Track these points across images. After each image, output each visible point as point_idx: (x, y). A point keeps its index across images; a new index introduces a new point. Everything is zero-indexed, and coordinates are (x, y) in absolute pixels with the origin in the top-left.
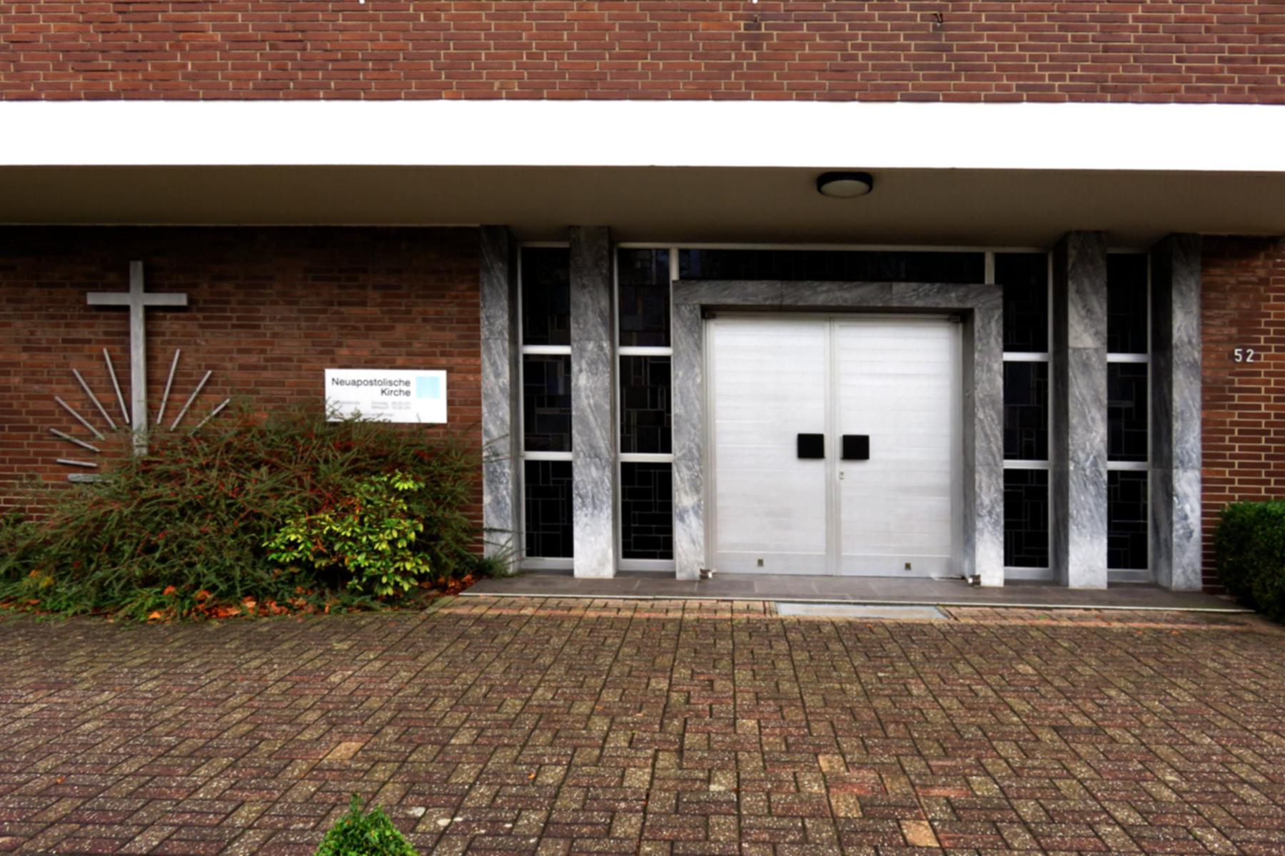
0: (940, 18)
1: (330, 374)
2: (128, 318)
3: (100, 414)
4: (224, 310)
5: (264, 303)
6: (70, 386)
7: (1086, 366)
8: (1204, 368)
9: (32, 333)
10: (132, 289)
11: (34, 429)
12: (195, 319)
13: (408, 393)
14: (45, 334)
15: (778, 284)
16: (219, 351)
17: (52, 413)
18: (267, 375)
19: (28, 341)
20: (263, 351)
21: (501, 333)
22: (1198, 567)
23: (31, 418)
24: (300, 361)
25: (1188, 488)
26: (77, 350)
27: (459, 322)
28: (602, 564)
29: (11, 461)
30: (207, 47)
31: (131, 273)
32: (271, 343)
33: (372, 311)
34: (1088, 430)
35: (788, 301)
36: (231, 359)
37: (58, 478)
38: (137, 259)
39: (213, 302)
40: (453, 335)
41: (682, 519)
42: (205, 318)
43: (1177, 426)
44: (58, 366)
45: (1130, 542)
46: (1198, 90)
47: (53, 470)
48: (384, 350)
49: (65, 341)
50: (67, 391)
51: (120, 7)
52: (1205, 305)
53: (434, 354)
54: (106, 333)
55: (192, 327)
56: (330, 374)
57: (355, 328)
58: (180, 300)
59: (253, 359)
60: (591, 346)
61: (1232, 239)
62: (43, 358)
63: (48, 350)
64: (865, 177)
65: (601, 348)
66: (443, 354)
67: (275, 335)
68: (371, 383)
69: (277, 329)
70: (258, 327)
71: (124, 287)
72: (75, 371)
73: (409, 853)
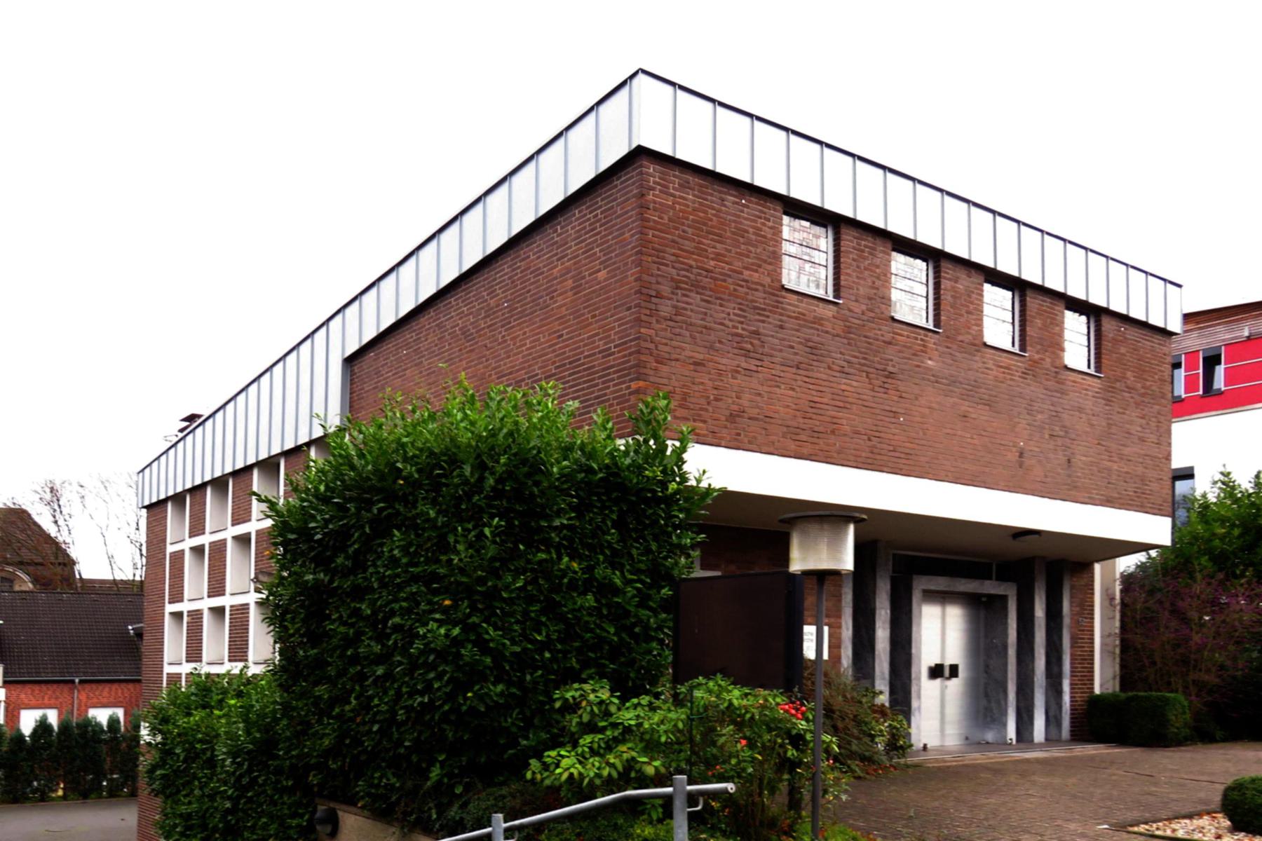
52: (1072, 597)
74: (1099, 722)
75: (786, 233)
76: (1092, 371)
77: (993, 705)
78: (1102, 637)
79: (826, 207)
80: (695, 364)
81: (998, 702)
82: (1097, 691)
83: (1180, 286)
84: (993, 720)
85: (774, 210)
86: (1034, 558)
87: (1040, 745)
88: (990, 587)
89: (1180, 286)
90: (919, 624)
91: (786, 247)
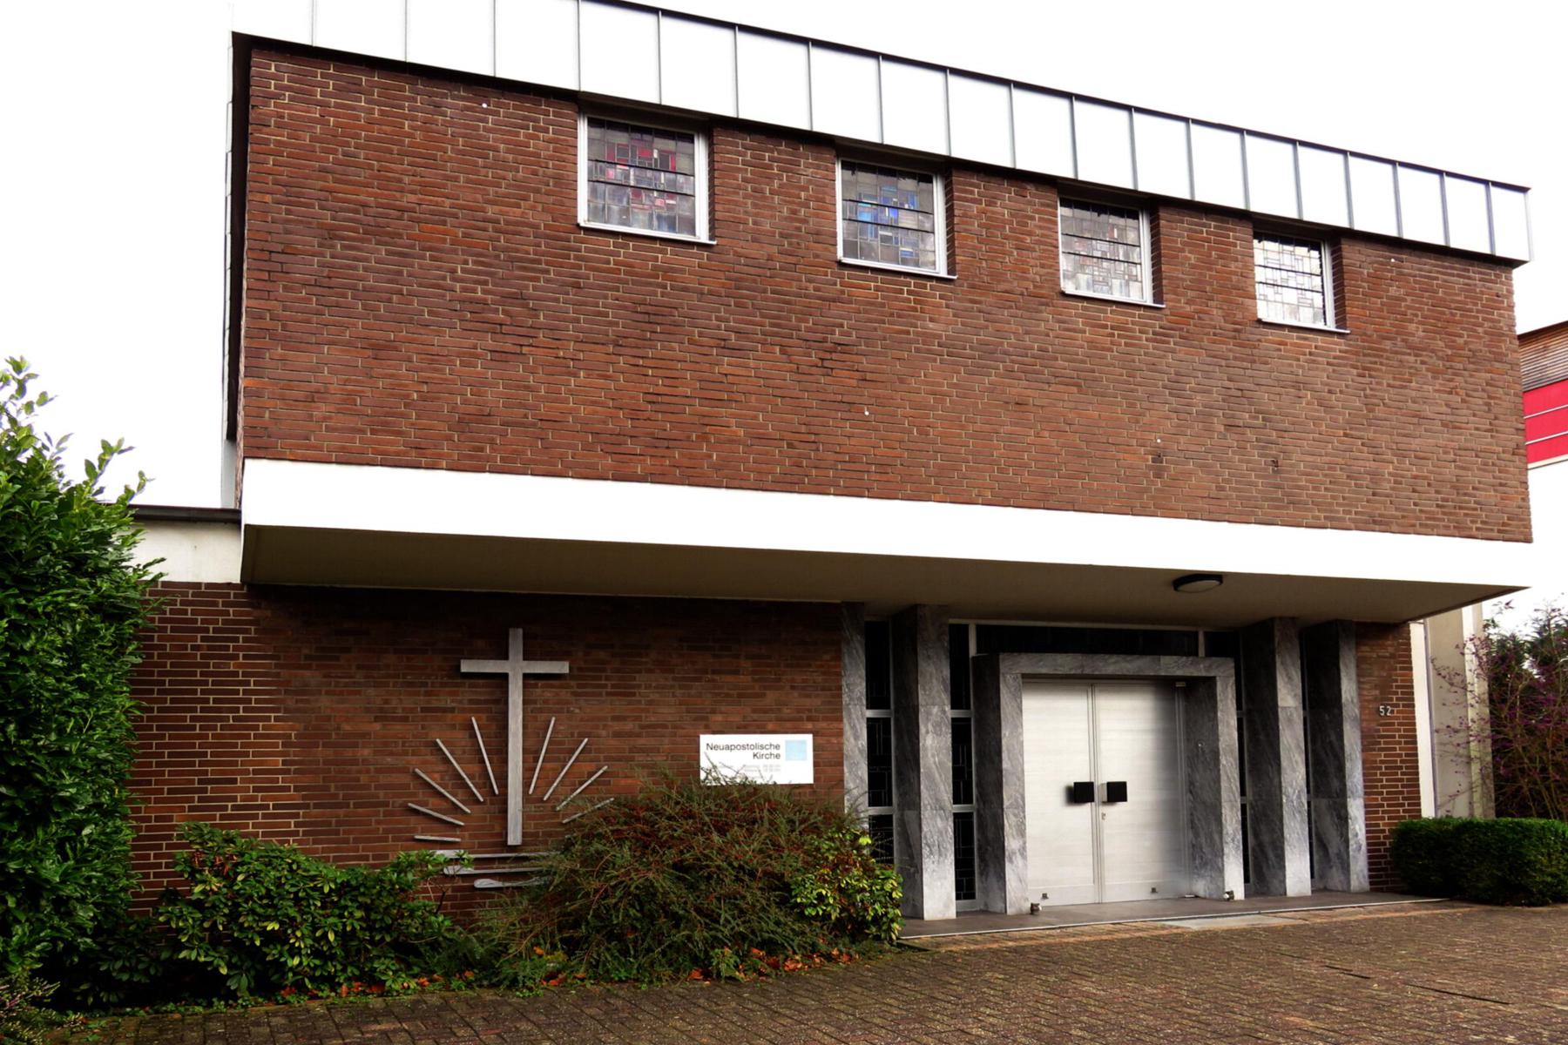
0: (1275, 463)
1: (705, 739)
5: (639, 672)
6: (429, 758)
7: (1290, 720)
8: (1362, 721)
9: (386, 702)
11: (386, 804)
12: (568, 687)
13: (778, 756)
15: (1079, 656)
18: (641, 741)
20: (638, 718)
21: (859, 699)
22: (1366, 872)
23: (381, 793)
24: (675, 727)
25: (1356, 809)
27: (823, 689)
28: (947, 906)
29: (356, 840)
30: (731, 441)
31: (511, 640)
33: (744, 679)
34: (1294, 770)
35: (1087, 671)
36: (605, 727)
40: (818, 702)
41: (1011, 861)
42: (579, 686)
43: (1348, 765)
44: (415, 736)
45: (1326, 854)
46: (1426, 526)
48: (755, 716)
50: (425, 762)
51: (650, 398)
52: (1360, 674)
53: (801, 719)
54: (471, 701)
55: (565, 694)
56: (705, 739)
57: (728, 695)
58: (562, 667)
59: (629, 726)
60: (935, 710)
61: (1374, 624)
62: (398, 727)
63: (405, 719)
64: (1218, 577)
65: (944, 712)
66: (809, 719)
67: (651, 703)
68: (744, 747)
69: (652, 697)
70: (634, 694)
71: (504, 655)
74: (1423, 863)
75: (1259, 258)
76: (1331, 326)
77: (1203, 840)
78: (1434, 731)
79: (1306, 218)
80: (374, 347)
81: (1210, 836)
82: (1428, 810)
83: (1523, 190)
84: (1204, 864)
85: (1238, 234)
86: (1272, 619)
87: (1300, 900)
88: (1198, 669)
89: (1523, 190)
90: (1018, 725)
91: (1260, 274)
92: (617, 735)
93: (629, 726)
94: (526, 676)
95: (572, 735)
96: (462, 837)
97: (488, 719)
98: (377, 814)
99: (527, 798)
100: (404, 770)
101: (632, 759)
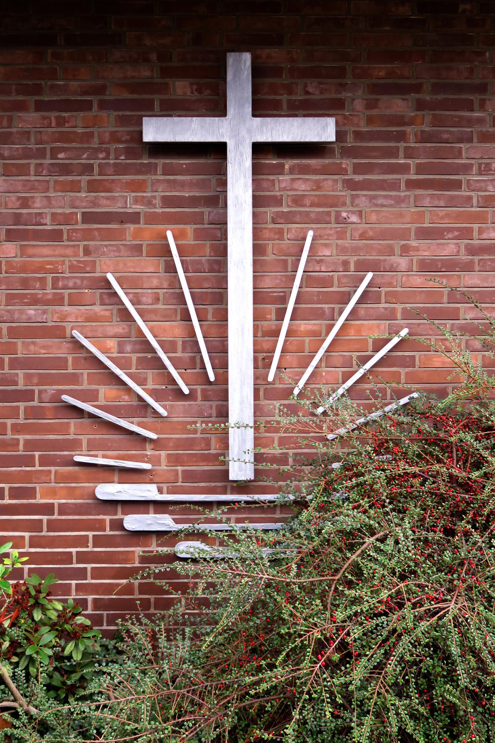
2: (221, 172)
3: (159, 364)
4: (393, 153)
6: (98, 309)
9: (25, 203)
10: (231, 110)
11: (27, 395)
14: (51, 203)
16: (383, 235)
17: (62, 363)
18: (471, 280)
19: (17, 219)
20: (466, 234)
26: (108, 236)
32: (480, 218)
36: (405, 250)
37: (71, 492)
38: (239, 48)
39: (373, 136)
42: (357, 169)
44: (73, 269)
47: (60, 478)
49: (88, 218)
54: (167, 201)
55: (332, 186)
58: (320, 130)
59: (448, 249)
62: (44, 252)
63: (56, 236)
70: (457, 185)
71: (218, 108)
72: (110, 277)
73: (290, 741)
92: (428, 267)
93: (448, 249)
94: (259, 149)
95: (346, 264)
96: (155, 461)
97: (198, 234)
98: (14, 414)
99: (262, 391)
100: (57, 332)
101: (454, 315)
